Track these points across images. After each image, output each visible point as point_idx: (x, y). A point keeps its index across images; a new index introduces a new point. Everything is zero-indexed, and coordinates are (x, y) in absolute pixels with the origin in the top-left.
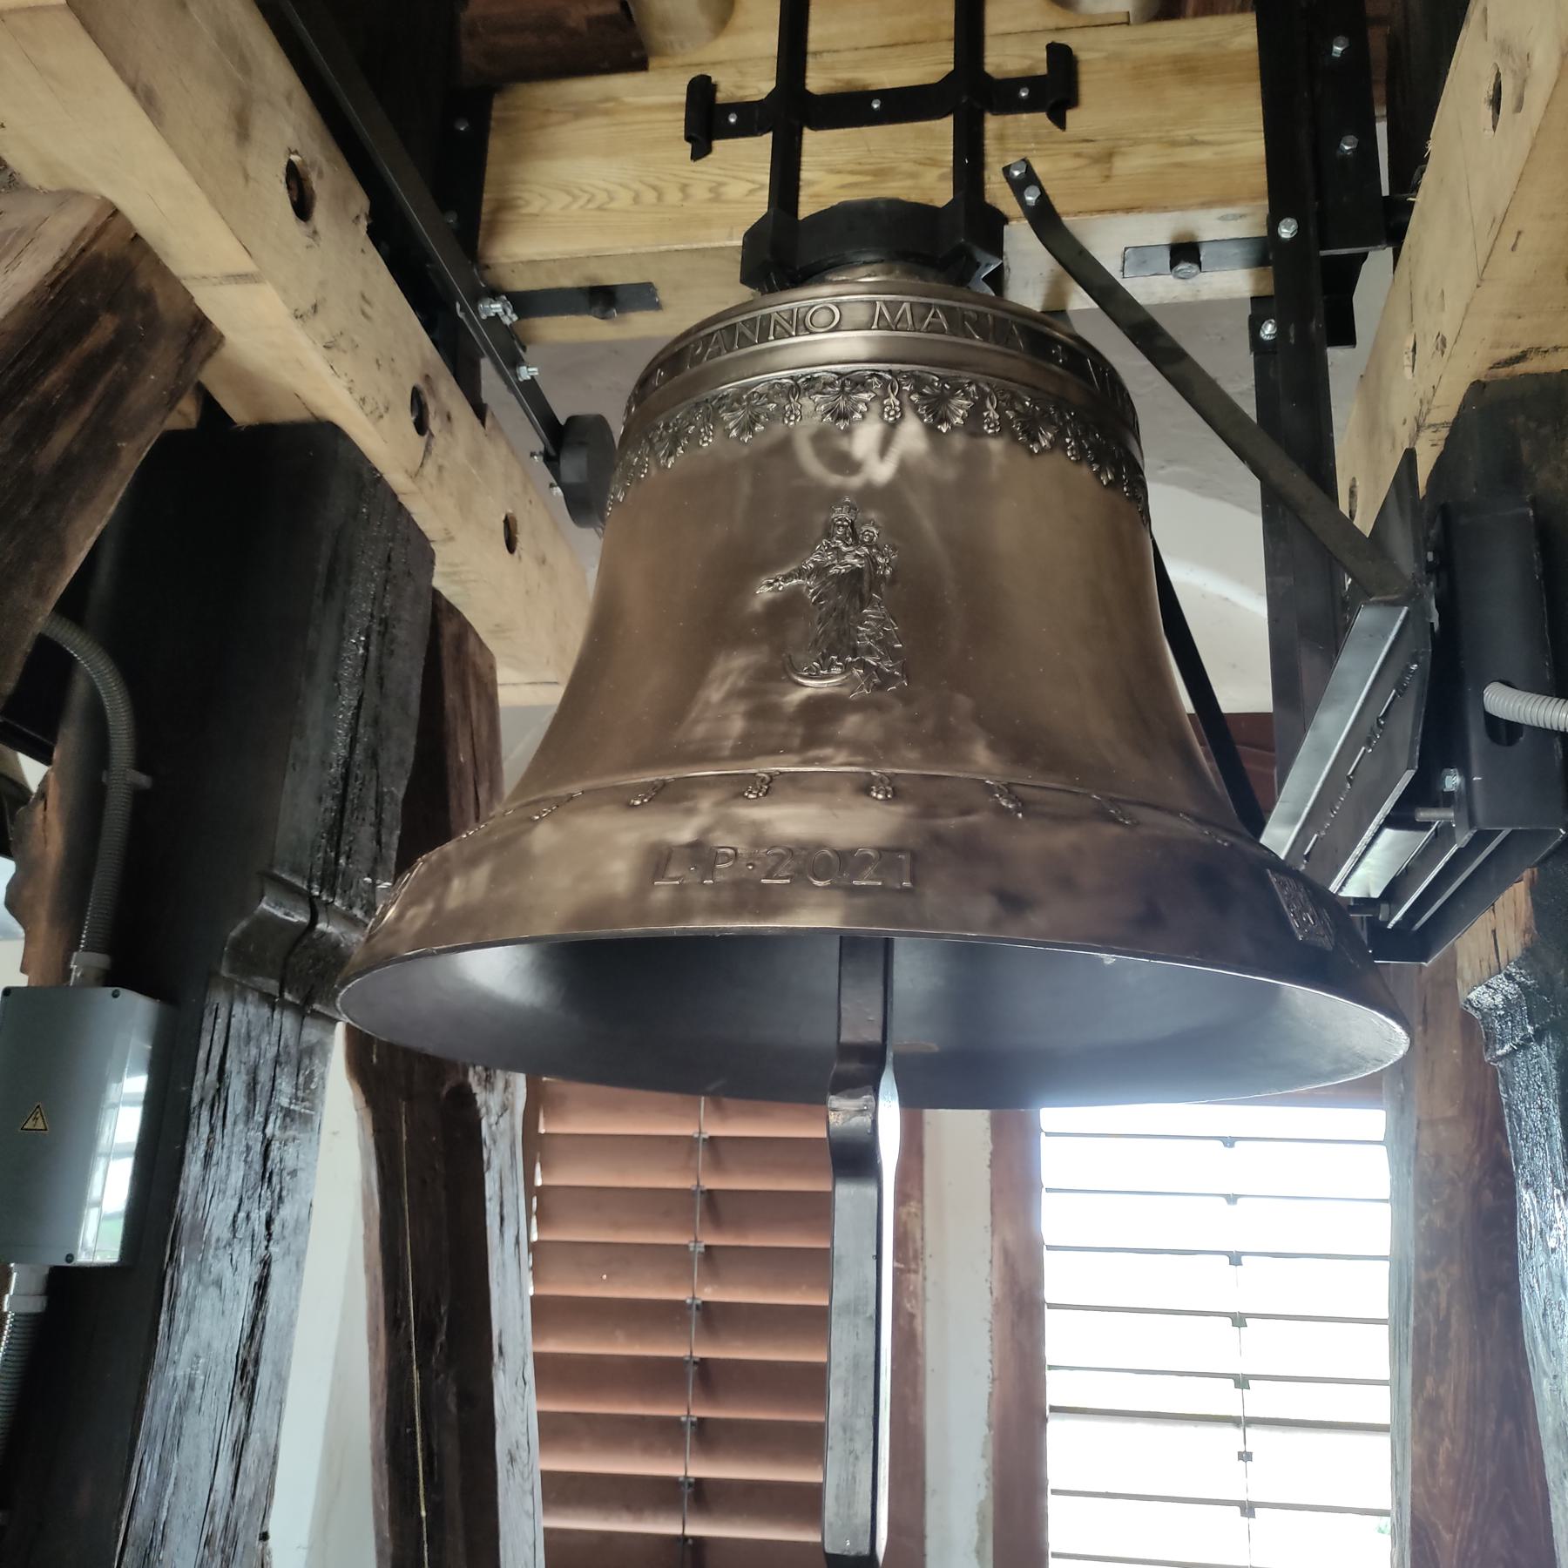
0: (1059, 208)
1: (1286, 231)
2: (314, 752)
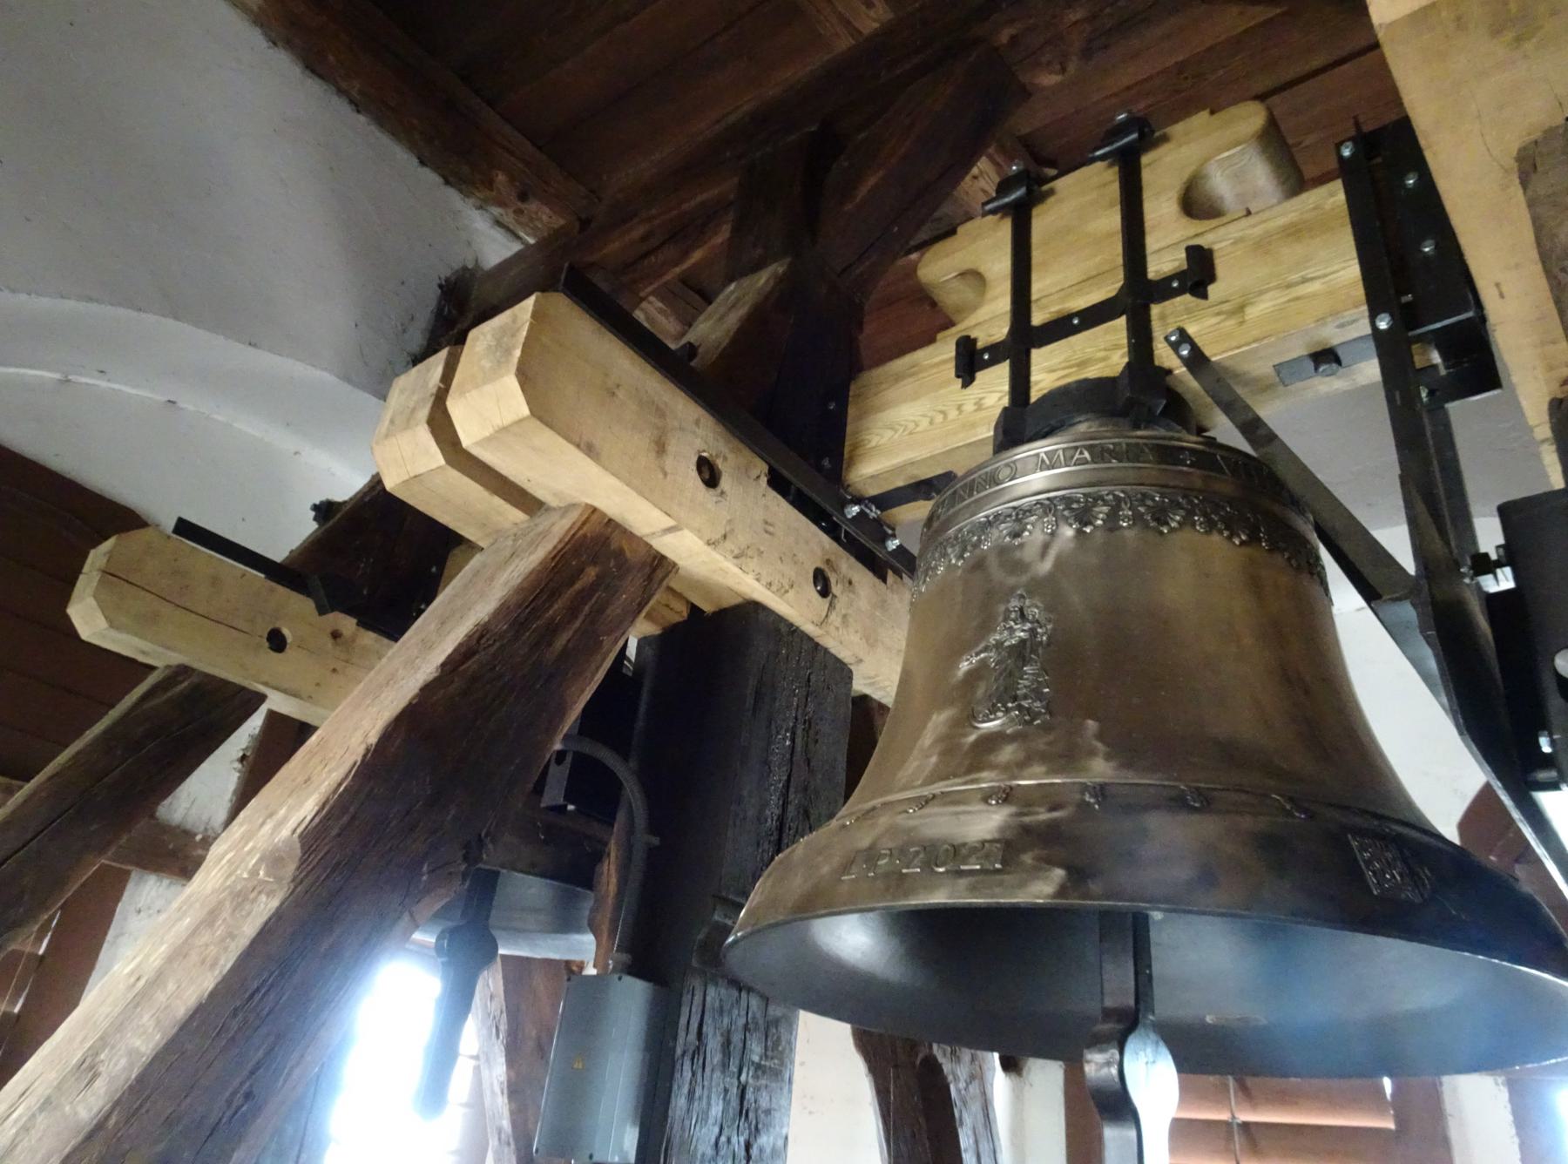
0: (1207, 353)
2: (751, 813)
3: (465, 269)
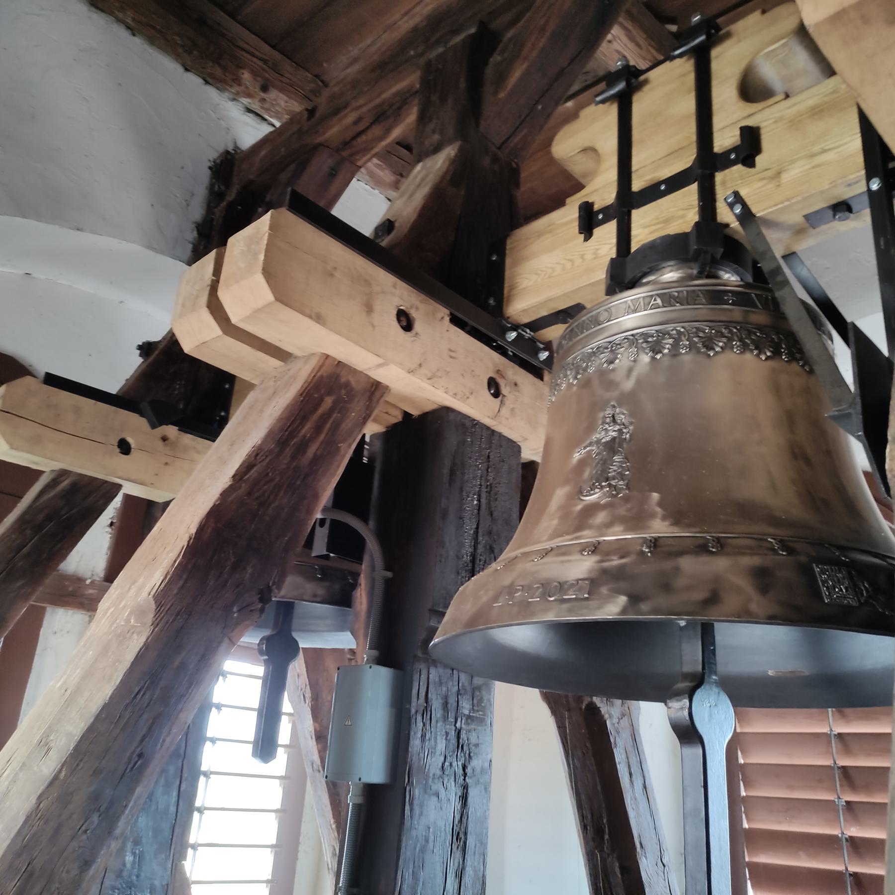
0: (754, 210)
1: (875, 186)
3: (227, 152)
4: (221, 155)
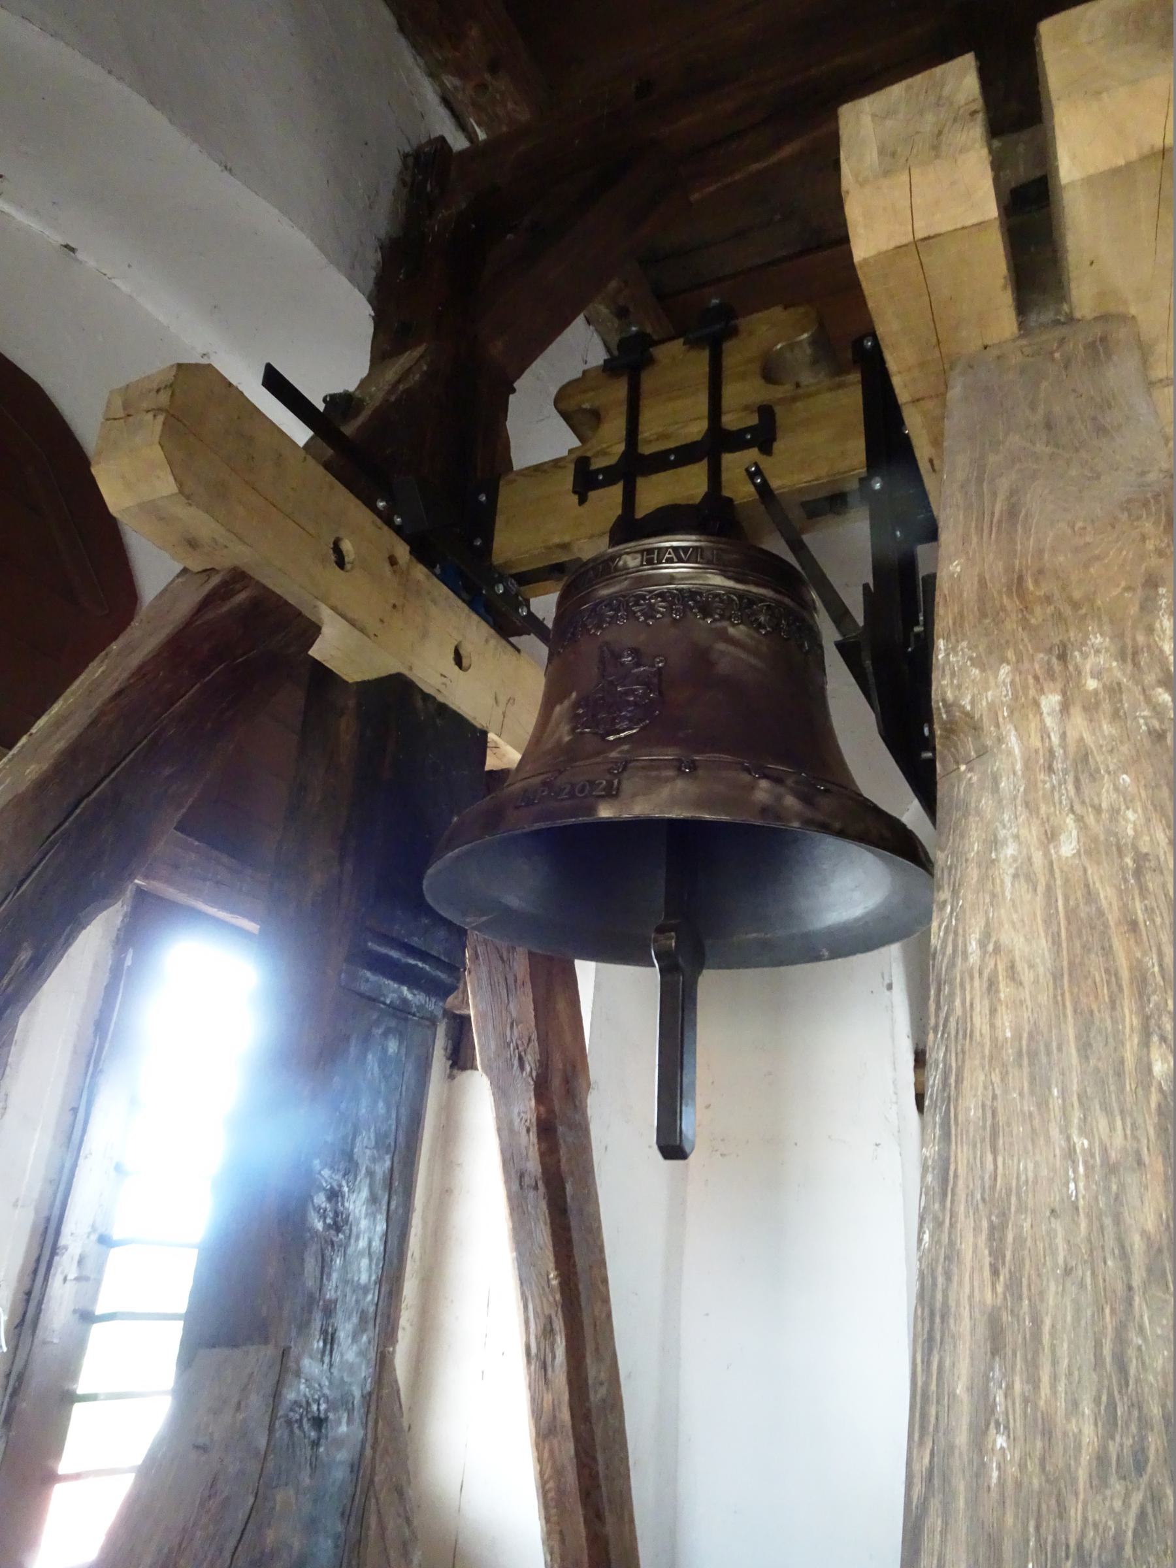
4: (430, 142)
